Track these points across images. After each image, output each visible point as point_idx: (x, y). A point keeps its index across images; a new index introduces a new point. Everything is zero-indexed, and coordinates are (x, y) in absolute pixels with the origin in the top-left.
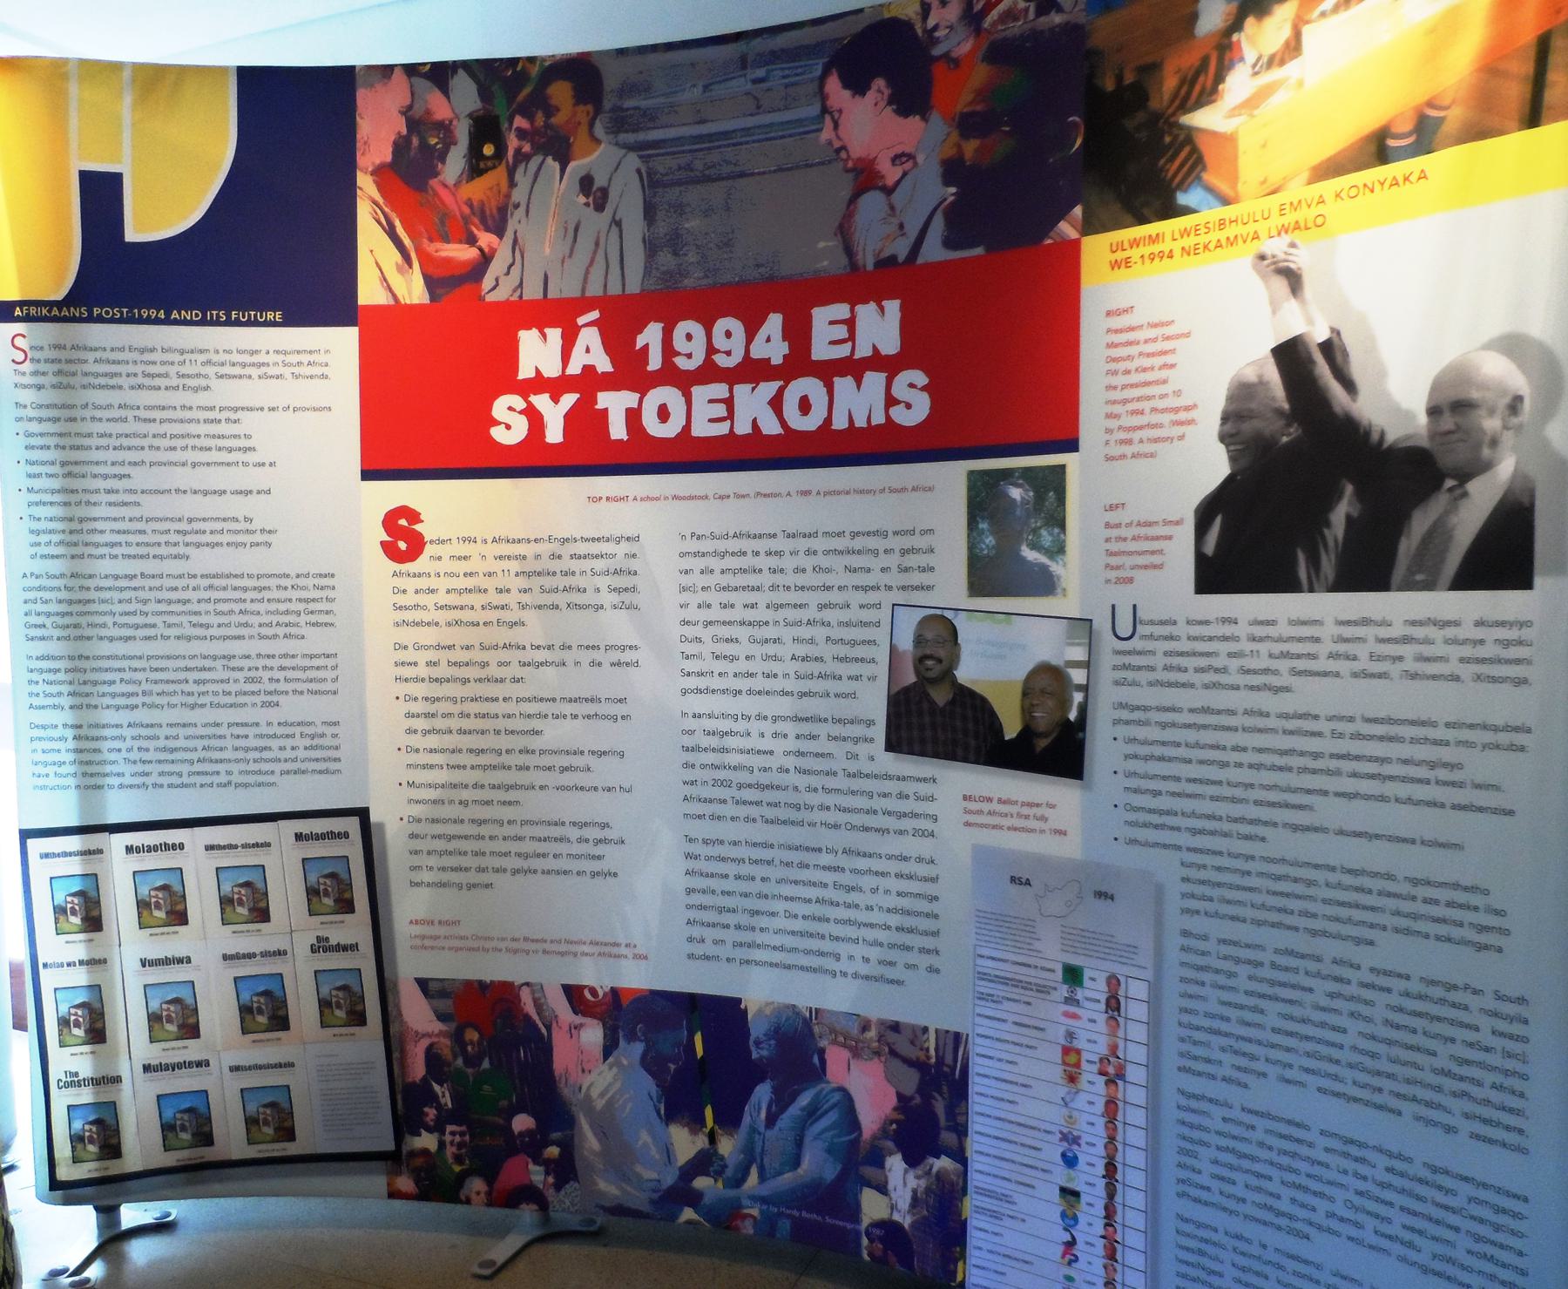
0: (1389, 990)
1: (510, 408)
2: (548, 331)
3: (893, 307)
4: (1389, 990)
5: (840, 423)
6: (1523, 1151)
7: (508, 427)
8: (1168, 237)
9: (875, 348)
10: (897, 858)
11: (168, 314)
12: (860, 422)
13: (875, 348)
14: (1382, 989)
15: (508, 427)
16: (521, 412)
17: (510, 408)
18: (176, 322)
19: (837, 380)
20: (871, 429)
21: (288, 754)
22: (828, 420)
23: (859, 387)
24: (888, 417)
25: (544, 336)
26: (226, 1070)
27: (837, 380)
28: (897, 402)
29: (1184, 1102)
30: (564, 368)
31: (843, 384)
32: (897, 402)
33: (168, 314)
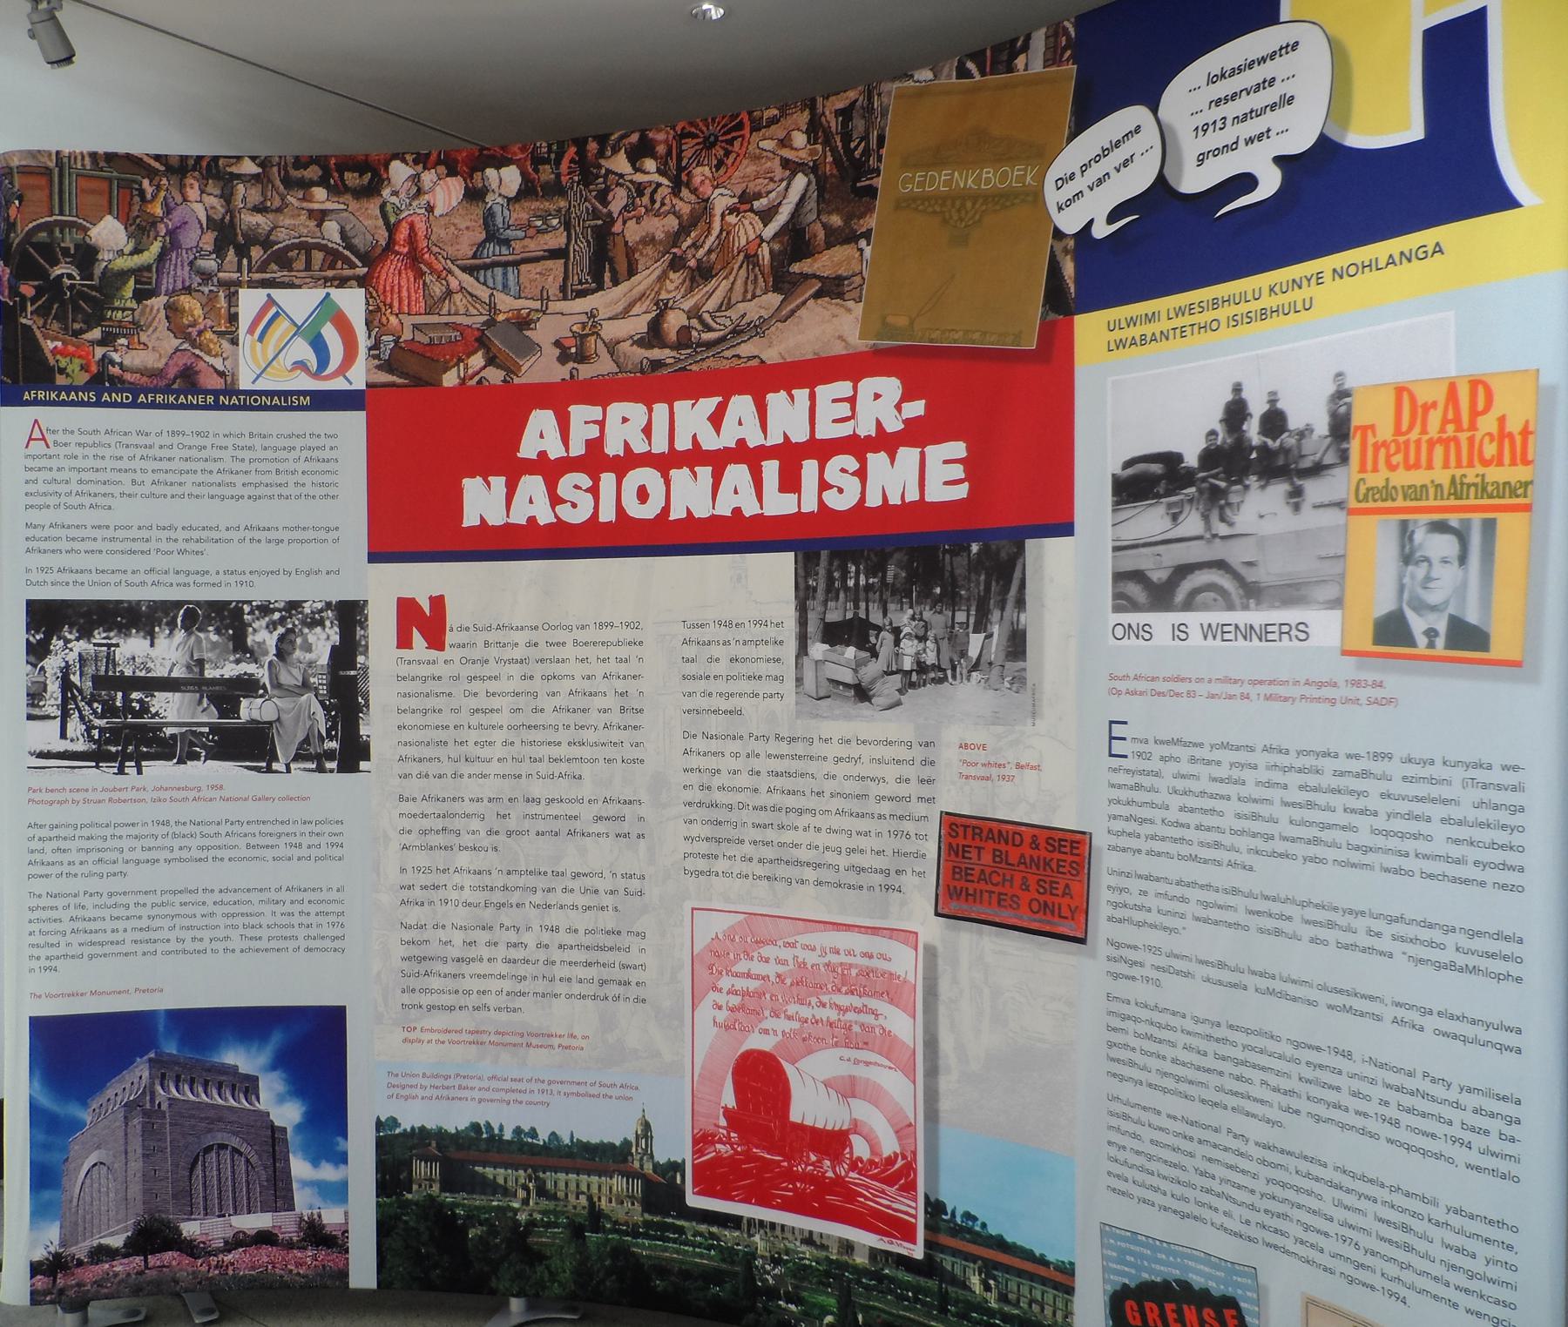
3: (470, 520)
5: (677, 513)
6: (1516, 1180)
7: (574, 505)
8: (1164, 316)
9: (482, 518)
11: (99, 396)
12: (895, 500)
13: (482, 518)
15: (574, 505)
18: (107, 405)
19: (869, 455)
20: (905, 507)
22: (666, 509)
23: (892, 462)
24: (556, 516)
26: (404, 653)
27: (869, 455)
28: (831, 487)
30: (567, 450)
31: (877, 460)
32: (831, 487)
33: (99, 396)
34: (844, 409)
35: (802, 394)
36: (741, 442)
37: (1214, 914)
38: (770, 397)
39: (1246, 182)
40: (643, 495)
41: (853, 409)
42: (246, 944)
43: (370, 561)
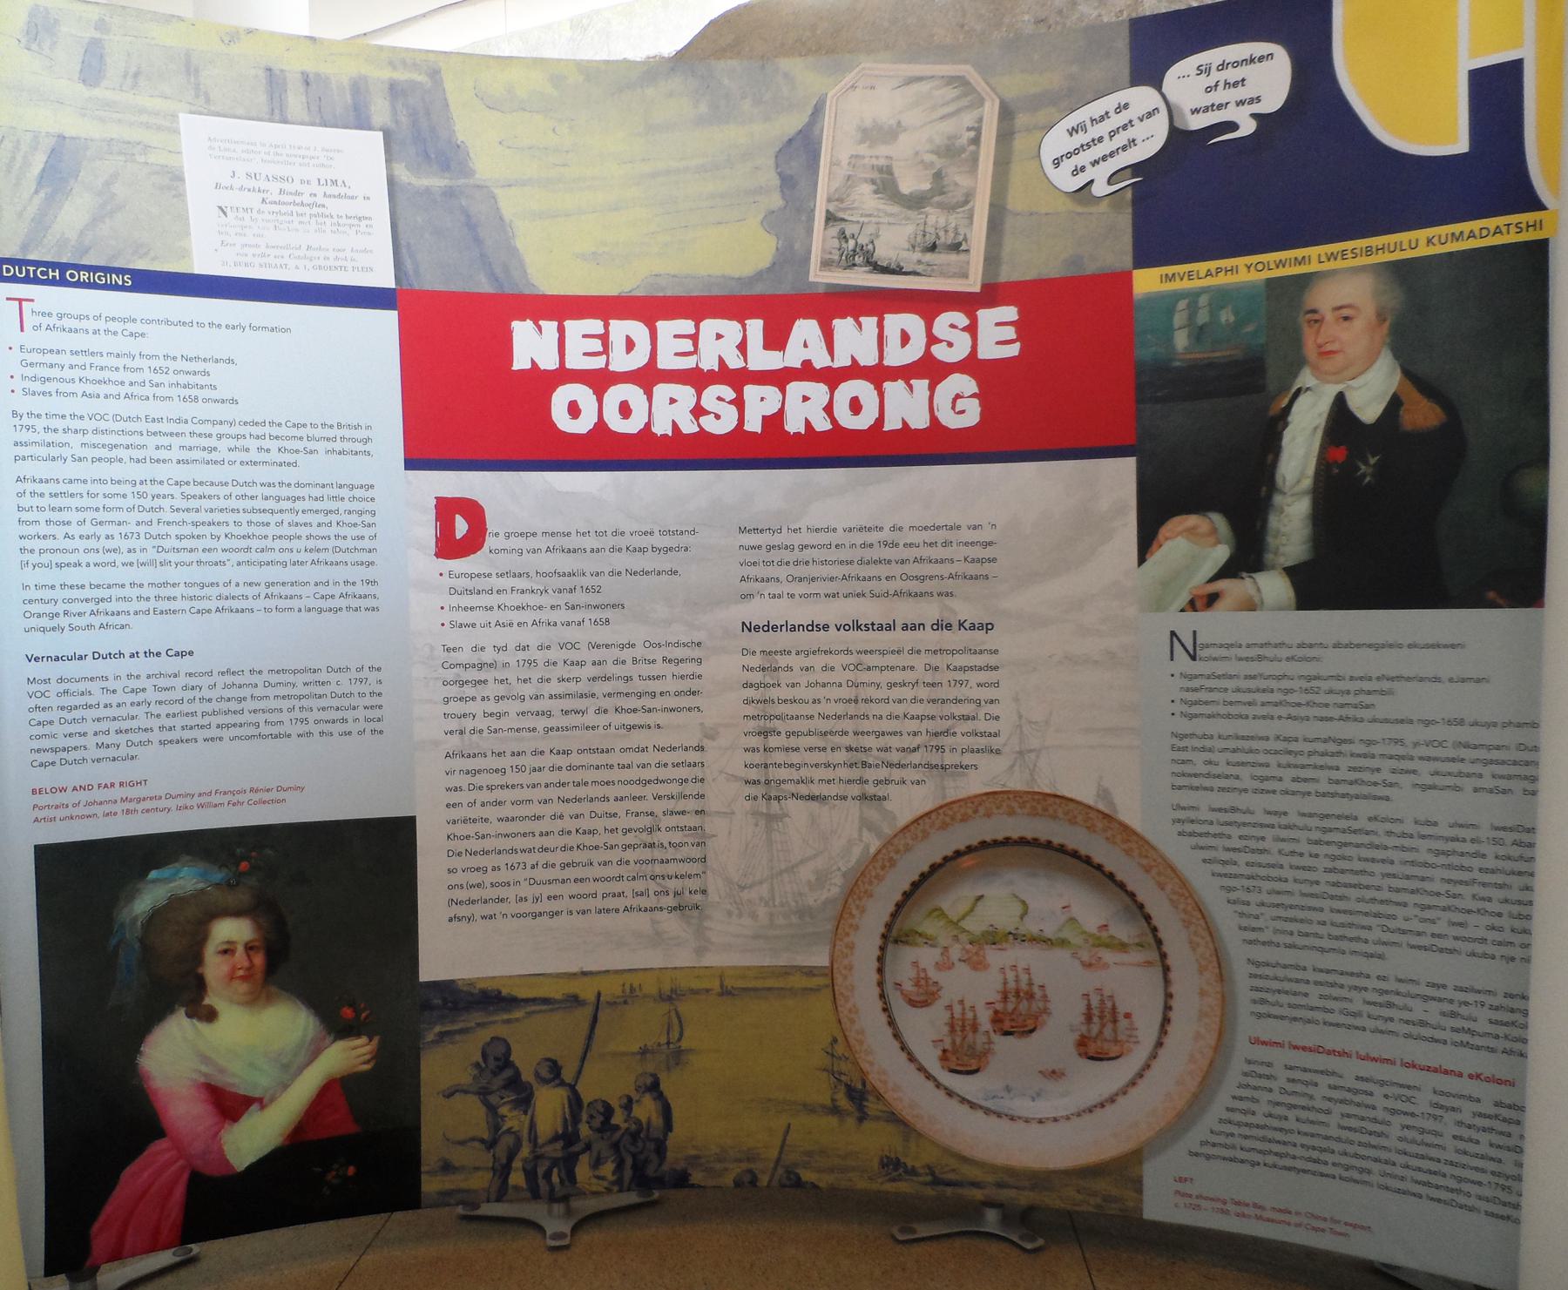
0: (1405, 905)
1: (719, 399)
2: (862, 319)
4: (1405, 905)
5: (892, 423)
7: (718, 417)
9: (533, 362)
10: (1429, 680)
13: (533, 362)
14: (1398, 904)
15: (718, 417)
16: (730, 402)
17: (719, 399)
21: (818, 661)
22: (880, 420)
25: (860, 325)
28: (707, 413)
29: (1254, 970)
34: (687, 345)
35: (870, 322)
36: (807, 364)
37: (1267, 785)
38: (837, 323)
39: (1232, 126)
40: (625, 410)
41: (696, 345)
42: (1257, 784)
43: (407, 468)
